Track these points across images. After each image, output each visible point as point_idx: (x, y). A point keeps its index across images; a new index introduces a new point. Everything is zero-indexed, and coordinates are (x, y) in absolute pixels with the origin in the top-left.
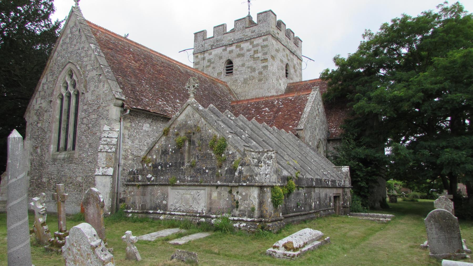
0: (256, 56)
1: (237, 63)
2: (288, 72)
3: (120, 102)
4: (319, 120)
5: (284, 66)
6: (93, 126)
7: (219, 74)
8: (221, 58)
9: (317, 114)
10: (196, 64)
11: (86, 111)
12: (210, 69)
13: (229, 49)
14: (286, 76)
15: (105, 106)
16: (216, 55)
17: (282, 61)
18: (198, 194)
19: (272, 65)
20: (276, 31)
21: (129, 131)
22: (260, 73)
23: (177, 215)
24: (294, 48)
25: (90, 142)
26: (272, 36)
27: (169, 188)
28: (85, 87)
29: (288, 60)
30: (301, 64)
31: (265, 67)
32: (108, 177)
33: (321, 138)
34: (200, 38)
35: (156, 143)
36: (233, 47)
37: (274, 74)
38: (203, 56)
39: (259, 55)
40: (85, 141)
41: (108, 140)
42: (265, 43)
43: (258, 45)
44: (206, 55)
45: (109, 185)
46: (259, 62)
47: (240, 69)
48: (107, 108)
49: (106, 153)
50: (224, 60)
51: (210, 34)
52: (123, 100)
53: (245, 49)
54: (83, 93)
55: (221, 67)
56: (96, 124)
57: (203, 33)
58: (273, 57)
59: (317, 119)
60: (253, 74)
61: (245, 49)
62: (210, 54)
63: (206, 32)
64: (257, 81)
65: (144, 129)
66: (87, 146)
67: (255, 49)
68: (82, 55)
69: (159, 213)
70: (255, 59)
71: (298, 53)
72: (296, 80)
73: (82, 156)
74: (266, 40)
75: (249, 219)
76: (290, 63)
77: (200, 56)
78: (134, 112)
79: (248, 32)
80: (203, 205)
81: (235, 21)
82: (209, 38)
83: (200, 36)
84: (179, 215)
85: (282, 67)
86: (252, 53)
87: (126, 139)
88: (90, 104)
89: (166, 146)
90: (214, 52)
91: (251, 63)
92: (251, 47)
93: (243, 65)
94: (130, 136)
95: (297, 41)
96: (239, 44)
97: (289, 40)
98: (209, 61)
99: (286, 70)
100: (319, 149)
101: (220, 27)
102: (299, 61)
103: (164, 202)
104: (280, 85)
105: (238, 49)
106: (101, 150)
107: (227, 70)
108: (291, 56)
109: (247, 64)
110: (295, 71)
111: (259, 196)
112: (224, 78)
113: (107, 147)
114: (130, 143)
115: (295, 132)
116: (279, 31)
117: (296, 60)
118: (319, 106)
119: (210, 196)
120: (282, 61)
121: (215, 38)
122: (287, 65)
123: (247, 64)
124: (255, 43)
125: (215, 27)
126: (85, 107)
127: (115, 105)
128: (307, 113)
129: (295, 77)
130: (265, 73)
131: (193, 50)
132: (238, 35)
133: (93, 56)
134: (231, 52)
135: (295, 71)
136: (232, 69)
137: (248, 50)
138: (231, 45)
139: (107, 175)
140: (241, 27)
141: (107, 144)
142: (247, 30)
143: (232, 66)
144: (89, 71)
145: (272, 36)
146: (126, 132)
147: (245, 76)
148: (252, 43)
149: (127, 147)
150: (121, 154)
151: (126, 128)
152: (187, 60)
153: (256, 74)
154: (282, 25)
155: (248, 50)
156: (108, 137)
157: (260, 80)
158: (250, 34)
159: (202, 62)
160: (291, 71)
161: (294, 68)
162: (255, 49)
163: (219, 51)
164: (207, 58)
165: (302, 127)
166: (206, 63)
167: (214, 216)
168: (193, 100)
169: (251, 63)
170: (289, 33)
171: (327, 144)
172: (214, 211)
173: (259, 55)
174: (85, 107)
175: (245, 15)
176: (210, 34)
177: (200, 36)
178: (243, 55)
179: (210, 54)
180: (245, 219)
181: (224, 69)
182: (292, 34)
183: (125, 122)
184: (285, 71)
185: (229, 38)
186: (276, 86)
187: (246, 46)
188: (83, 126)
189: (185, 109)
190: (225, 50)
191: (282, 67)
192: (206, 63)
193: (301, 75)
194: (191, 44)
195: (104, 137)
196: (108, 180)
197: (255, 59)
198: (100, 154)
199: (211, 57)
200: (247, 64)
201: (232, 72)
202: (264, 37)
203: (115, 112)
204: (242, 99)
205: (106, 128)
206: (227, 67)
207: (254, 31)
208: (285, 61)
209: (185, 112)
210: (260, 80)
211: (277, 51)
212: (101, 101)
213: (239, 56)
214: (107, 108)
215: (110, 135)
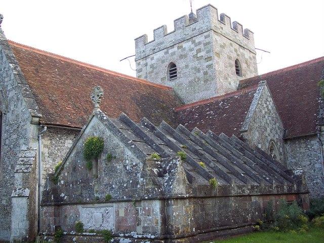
0: (199, 55)
1: (180, 65)
2: (239, 69)
3: (37, 119)
4: (270, 118)
5: (234, 63)
6: (14, 147)
7: (162, 79)
8: (163, 62)
9: (266, 112)
10: (139, 71)
11: (7, 131)
12: (153, 75)
13: (171, 51)
14: (237, 73)
15: (24, 125)
16: (158, 60)
17: (230, 58)
18: (107, 211)
19: (217, 63)
20: (219, 25)
21: (49, 148)
22: (205, 73)
23: (88, 235)
24: (244, 42)
25: (12, 163)
26: (214, 31)
27: (80, 207)
28: (7, 107)
29: (238, 55)
30: (254, 58)
31: (210, 66)
32: (24, 198)
33: (275, 139)
34: (141, 44)
35: (66, 160)
36: (175, 49)
37: (220, 72)
38: (145, 62)
39: (203, 54)
40: (8, 163)
41: (25, 159)
42: (207, 40)
43: (200, 43)
44: (149, 60)
45: (26, 206)
46: (202, 61)
47: (185, 70)
48: (24, 127)
49: (22, 174)
50: (167, 63)
51: (150, 38)
52: (40, 117)
53: (187, 49)
54: (5, 114)
55: (164, 71)
56: (17, 145)
57: (144, 37)
58: (218, 54)
59: (266, 117)
60: (198, 75)
61: (187, 49)
62: (152, 59)
63: (147, 36)
64: (202, 82)
65: (66, 145)
66: (10, 168)
67: (198, 47)
68: (4, 76)
69: (72, 235)
70: (199, 59)
71: (251, 46)
72: (250, 75)
73: (5, 179)
74: (209, 36)
75: (153, 237)
76: (240, 58)
77: (142, 62)
78: (53, 128)
79: (189, 31)
80: (112, 223)
81: (175, 21)
82: (150, 42)
83: (141, 40)
84: (90, 235)
85: (230, 63)
86: (195, 52)
87: (46, 158)
88: (11, 125)
89: (76, 162)
90: (156, 56)
91: (196, 64)
92: (193, 46)
93: (187, 66)
94: (50, 154)
95: (247, 34)
96: (180, 45)
97: (236, 34)
98: (152, 66)
99: (236, 67)
100: (274, 152)
101: (160, 29)
102: (252, 55)
103: (77, 222)
104: (230, 84)
105: (180, 50)
106: (17, 170)
107: (171, 74)
108: (241, 50)
109: (191, 64)
110: (248, 66)
111: (163, 211)
112: (171, 84)
113: (23, 167)
114: (51, 161)
115: (239, 134)
116: (222, 26)
117: (247, 55)
118: (268, 103)
119: (117, 213)
120: (230, 58)
121: (156, 41)
122: (237, 62)
123: (191, 65)
124: (197, 41)
125: (155, 30)
126: (7, 128)
127: (32, 123)
128: (252, 112)
129: (248, 72)
130: (210, 73)
131: (135, 57)
132: (179, 36)
133: (12, 75)
134: (174, 53)
135: (248, 66)
136: (176, 73)
137: (191, 50)
138: (172, 47)
139: (23, 197)
140: (181, 26)
141: (24, 164)
142: (187, 29)
143: (176, 69)
144: (10, 91)
145: (214, 31)
146: (46, 150)
147: (190, 79)
148: (194, 42)
149: (48, 166)
150: (41, 174)
151: (45, 146)
152: (128, 70)
153: (201, 75)
154: (226, 18)
155: (191, 50)
156: (25, 157)
157: (206, 81)
158: (190, 33)
159: (144, 69)
160: (243, 66)
161: (246, 63)
162: (198, 47)
163: (161, 54)
164: (149, 64)
165: (247, 129)
166: (149, 69)
167: (122, 235)
168: (99, 110)
169: (196, 64)
170: (236, 27)
171: (283, 145)
172: (122, 230)
173: (203, 54)
174: (7, 128)
175: (188, 13)
176: (150, 38)
177: (141, 40)
178: (185, 56)
179: (152, 59)
180: (149, 236)
181: (167, 74)
182: (240, 27)
183: (43, 140)
184: (234, 68)
185: (170, 40)
186: (226, 83)
187: (186, 45)
188: (6, 147)
189: (91, 121)
190: (167, 53)
191: (230, 63)
192: (149, 69)
193: (256, 70)
194: (133, 51)
195: (21, 157)
196: (24, 201)
197: (199, 59)
198: (16, 175)
199: (153, 62)
200: (191, 64)
201: (176, 76)
202: (205, 34)
203: (32, 130)
204: (189, 103)
205: (24, 147)
206: (170, 71)
207: (195, 29)
208: (234, 56)
209: (91, 124)
210: (206, 81)
211: (223, 47)
212: (20, 120)
213: (181, 57)
214: (24, 127)
215: (28, 155)
